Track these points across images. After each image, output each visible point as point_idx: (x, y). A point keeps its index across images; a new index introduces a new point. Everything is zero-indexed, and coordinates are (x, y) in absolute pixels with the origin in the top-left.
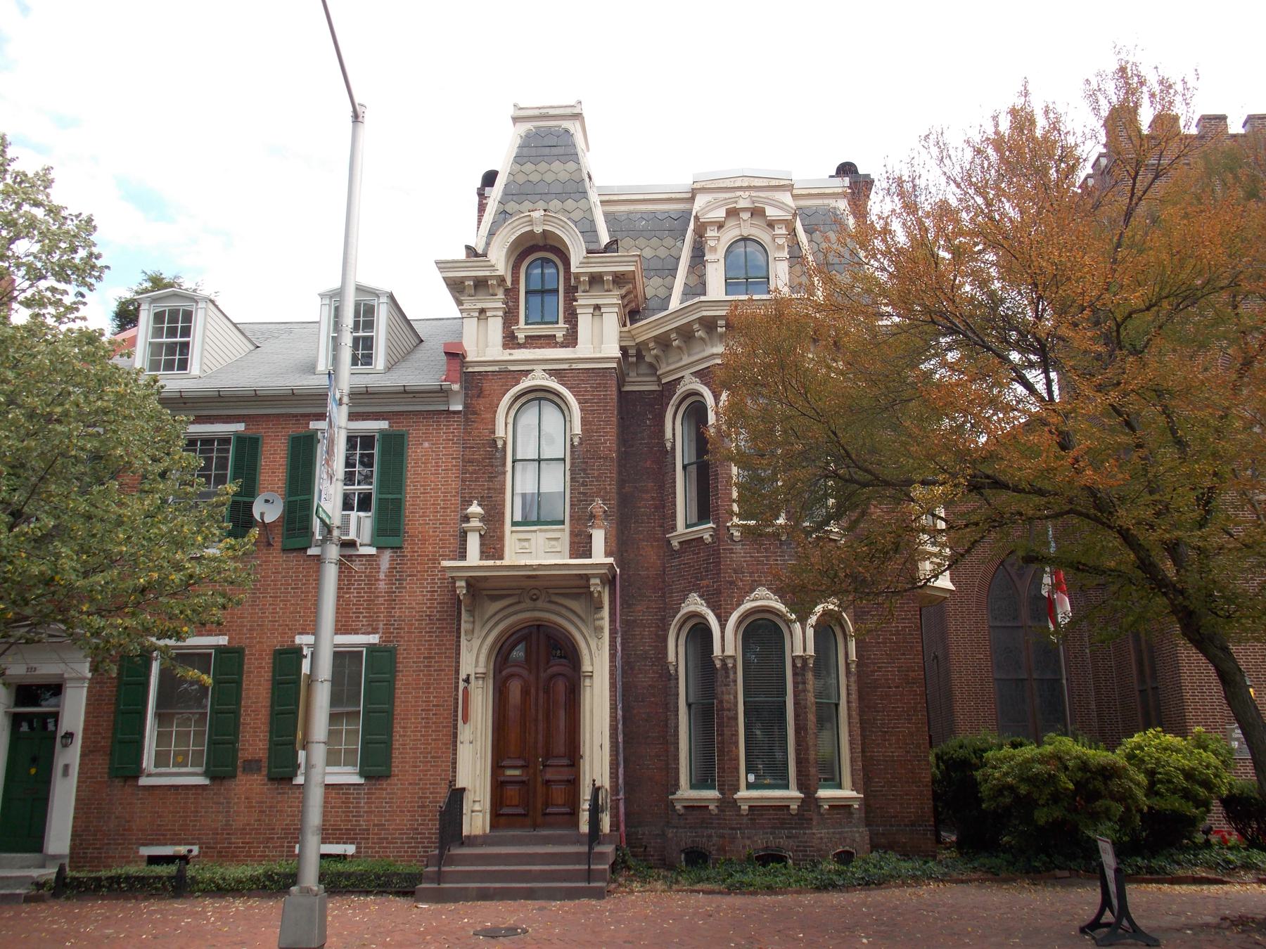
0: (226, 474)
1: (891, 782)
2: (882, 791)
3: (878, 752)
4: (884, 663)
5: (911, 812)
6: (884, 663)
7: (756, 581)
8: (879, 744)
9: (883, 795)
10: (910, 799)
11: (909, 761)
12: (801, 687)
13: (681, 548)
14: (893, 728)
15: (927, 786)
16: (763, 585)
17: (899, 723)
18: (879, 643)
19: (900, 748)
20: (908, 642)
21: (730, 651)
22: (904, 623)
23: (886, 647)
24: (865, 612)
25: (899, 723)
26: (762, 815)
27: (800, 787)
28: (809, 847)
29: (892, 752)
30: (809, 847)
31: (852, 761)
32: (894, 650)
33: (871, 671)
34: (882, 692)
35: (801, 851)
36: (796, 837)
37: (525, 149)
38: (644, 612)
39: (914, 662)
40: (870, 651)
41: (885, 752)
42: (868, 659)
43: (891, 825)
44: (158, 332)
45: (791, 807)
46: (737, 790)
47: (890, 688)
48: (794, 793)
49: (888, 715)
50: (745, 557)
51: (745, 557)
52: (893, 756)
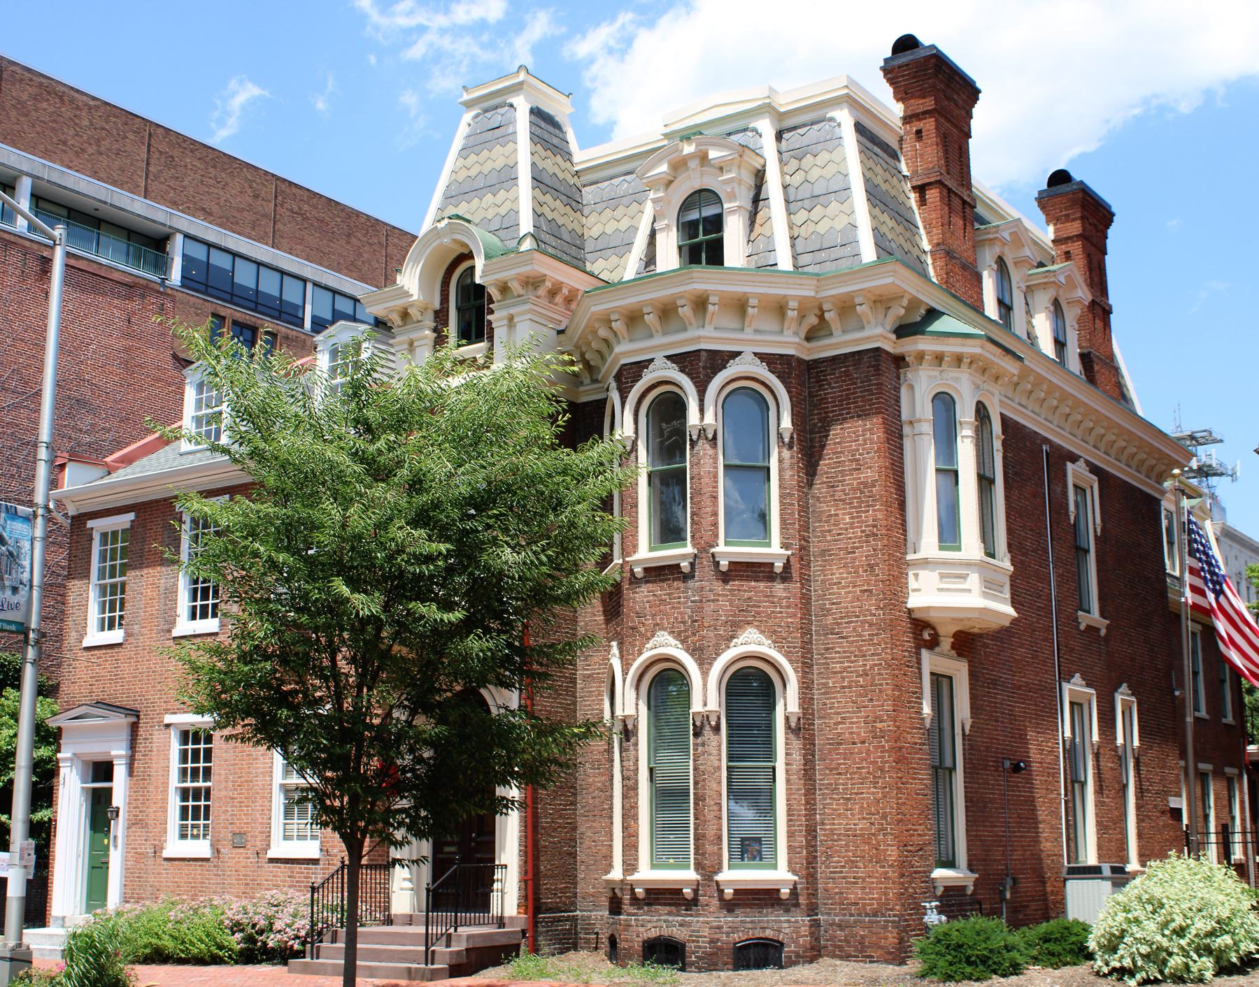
0: (685, 468)
1: (852, 862)
2: (842, 872)
3: (840, 824)
4: (849, 712)
5: (873, 899)
6: (849, 712)
7: (658, 625)
8: (839, 814)
9: (844, 878)
10: (873, 883)
11: (873, 835)
12: (700, 749)
13: (729, 570)
14: (856, 794)
15: (892, 866)
16: (664, 629)
17: (863, 788)
18: (844, 687)
19: (864, 818)
20: (876, 685)
21: (630, 711)
22: (873, 660)
23: (850, 692)
24: (828, 649)
25: (863, 788)
26: (658, 899)
27: (699, 866)
28: (701, 937)
29: (855, 825)
30: (701, 937)
31: (791, 835)
32: (861, 696)
33: (835, 724)
34: (845, 749)
35: (693, 941)
36: (689, 924)
37: (510, 131)
38: (600, 664)
39: (883, 710)
40: (834, 698)
41: (847, 824)
42: (831, 708)
43: (851, 915)
44: (199, 408)
45: (782, 891)
46: (719, 869)
47: (854, 743)
48: (691, 874)
49: (852, 779)
50: (648, 596)
51: (648, 596)
52: (856, 830)
